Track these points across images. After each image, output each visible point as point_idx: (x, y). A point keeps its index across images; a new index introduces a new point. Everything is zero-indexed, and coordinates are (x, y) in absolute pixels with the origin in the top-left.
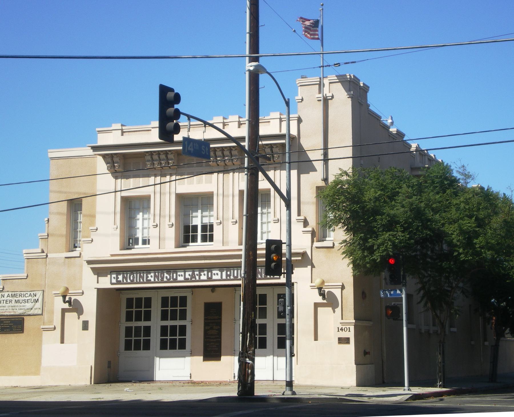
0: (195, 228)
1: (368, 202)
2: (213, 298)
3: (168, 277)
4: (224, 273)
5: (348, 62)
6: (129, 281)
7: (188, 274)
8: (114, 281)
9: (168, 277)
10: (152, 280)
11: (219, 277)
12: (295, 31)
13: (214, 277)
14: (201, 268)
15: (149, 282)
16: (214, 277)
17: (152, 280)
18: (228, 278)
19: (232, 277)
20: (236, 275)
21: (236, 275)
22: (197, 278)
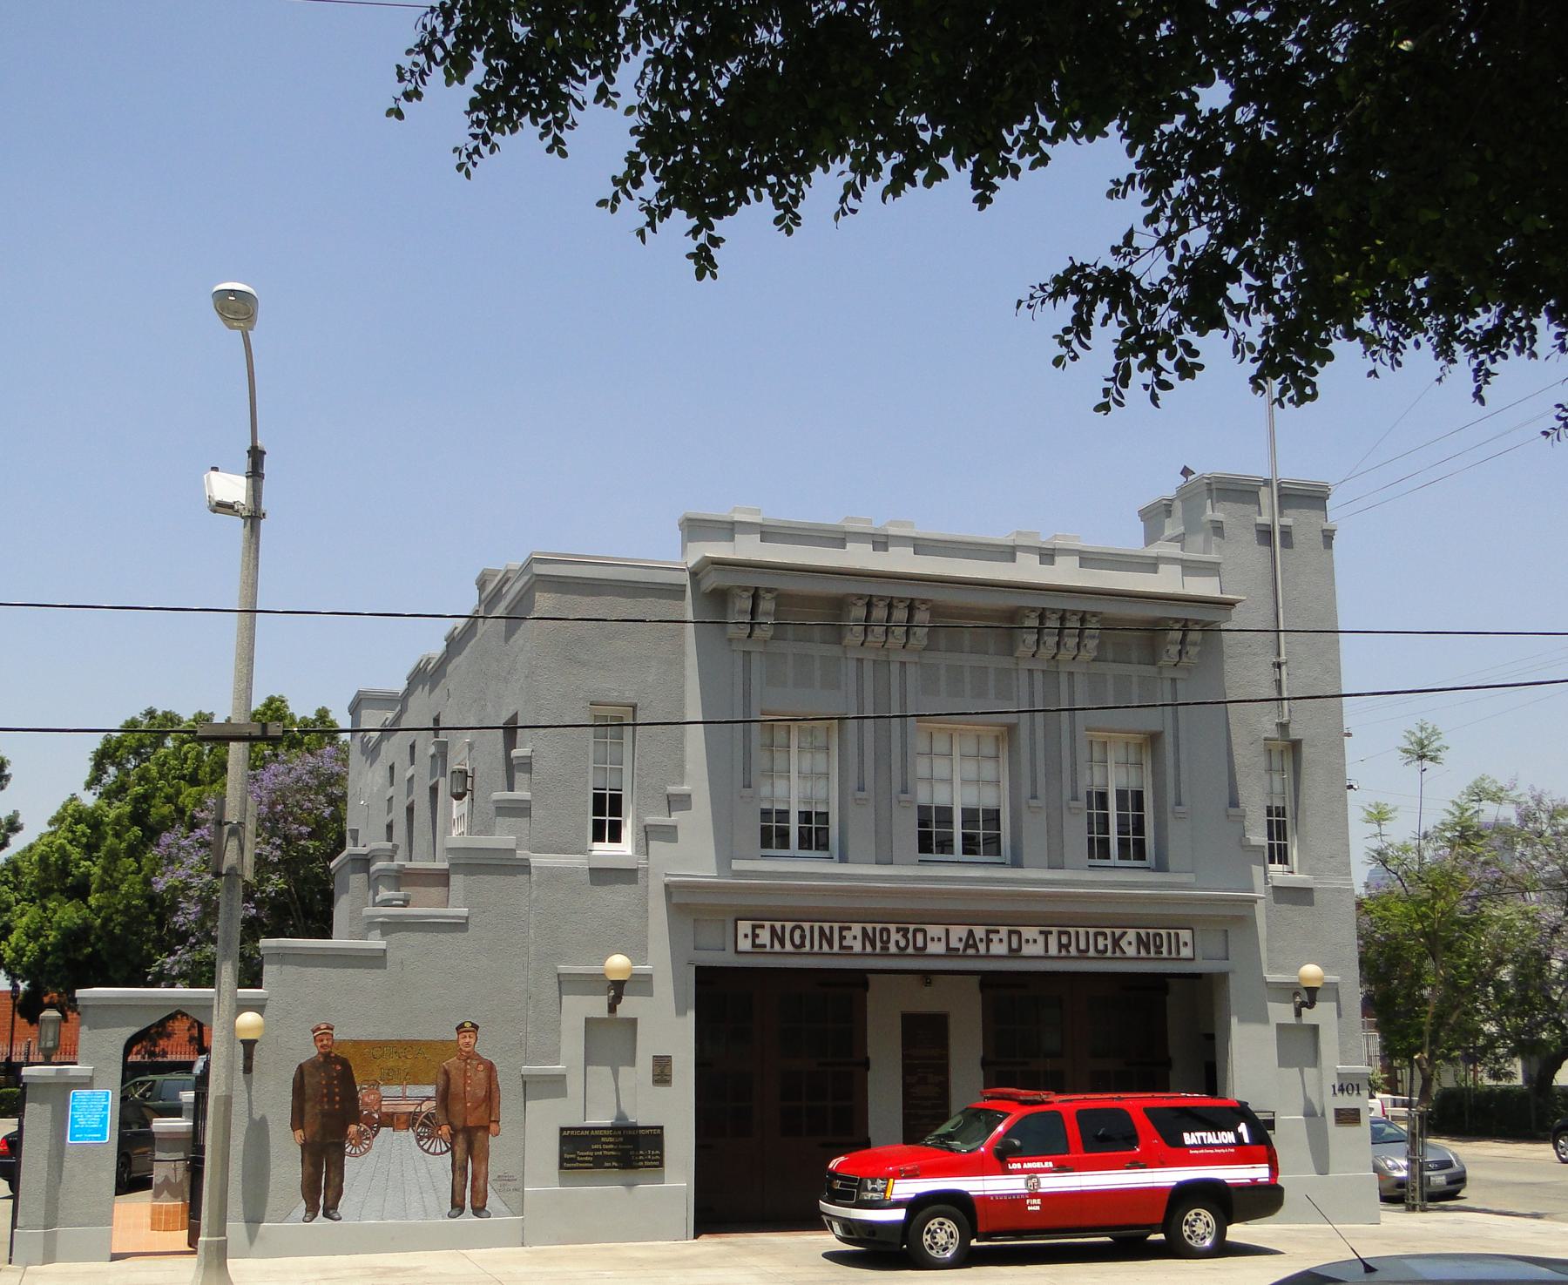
0: (947, 811)
1: (1478, 898)
2: (926, 1001)
3: (903, 943)
4: (1053, 940)
5: (267, 468)
6: (789, 947)
7: (958, 932)
8: (745, 945)
9: (903, 943)
10: (857, 947)
11: (1038, 949)
12: (236, 309)
13: (1027, 950)
14: (992, 921)
15: (846, 950)
16: (1027, 950)
17: (857, 947)
18: (1064, 953)
19: (910, 950)
20: (1082, 946)
21: (1082, 946)
22: (982, 948)
